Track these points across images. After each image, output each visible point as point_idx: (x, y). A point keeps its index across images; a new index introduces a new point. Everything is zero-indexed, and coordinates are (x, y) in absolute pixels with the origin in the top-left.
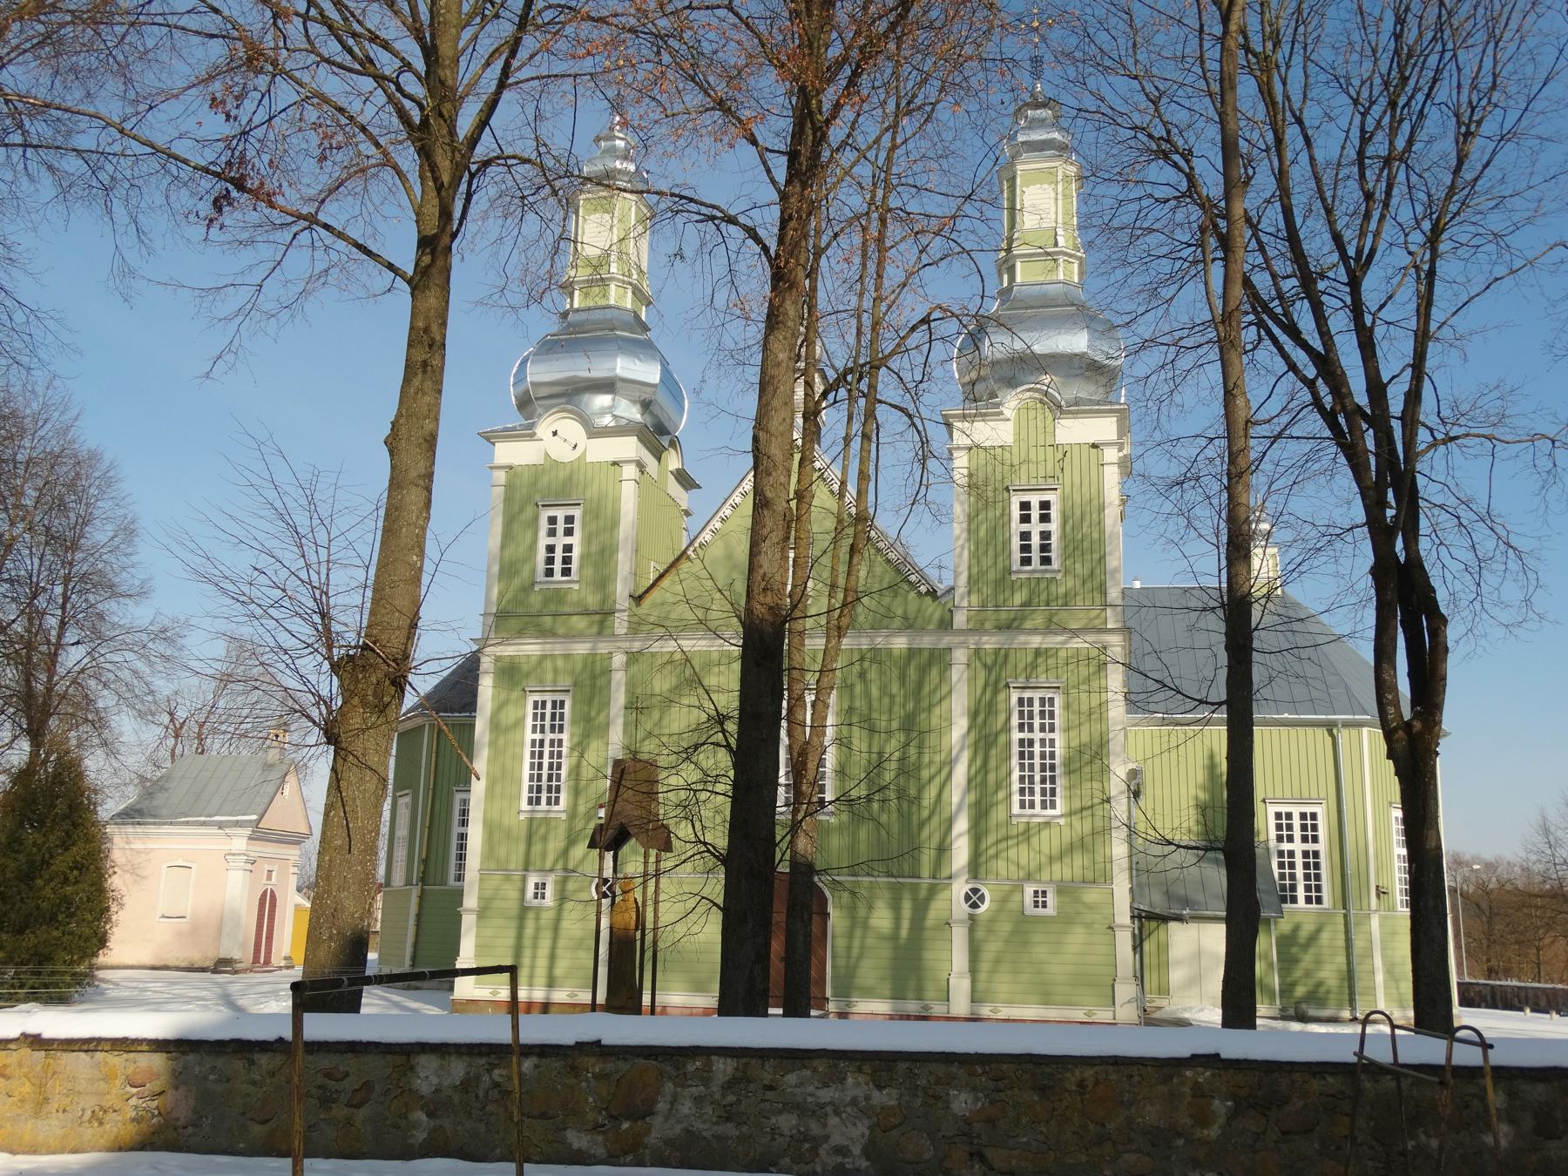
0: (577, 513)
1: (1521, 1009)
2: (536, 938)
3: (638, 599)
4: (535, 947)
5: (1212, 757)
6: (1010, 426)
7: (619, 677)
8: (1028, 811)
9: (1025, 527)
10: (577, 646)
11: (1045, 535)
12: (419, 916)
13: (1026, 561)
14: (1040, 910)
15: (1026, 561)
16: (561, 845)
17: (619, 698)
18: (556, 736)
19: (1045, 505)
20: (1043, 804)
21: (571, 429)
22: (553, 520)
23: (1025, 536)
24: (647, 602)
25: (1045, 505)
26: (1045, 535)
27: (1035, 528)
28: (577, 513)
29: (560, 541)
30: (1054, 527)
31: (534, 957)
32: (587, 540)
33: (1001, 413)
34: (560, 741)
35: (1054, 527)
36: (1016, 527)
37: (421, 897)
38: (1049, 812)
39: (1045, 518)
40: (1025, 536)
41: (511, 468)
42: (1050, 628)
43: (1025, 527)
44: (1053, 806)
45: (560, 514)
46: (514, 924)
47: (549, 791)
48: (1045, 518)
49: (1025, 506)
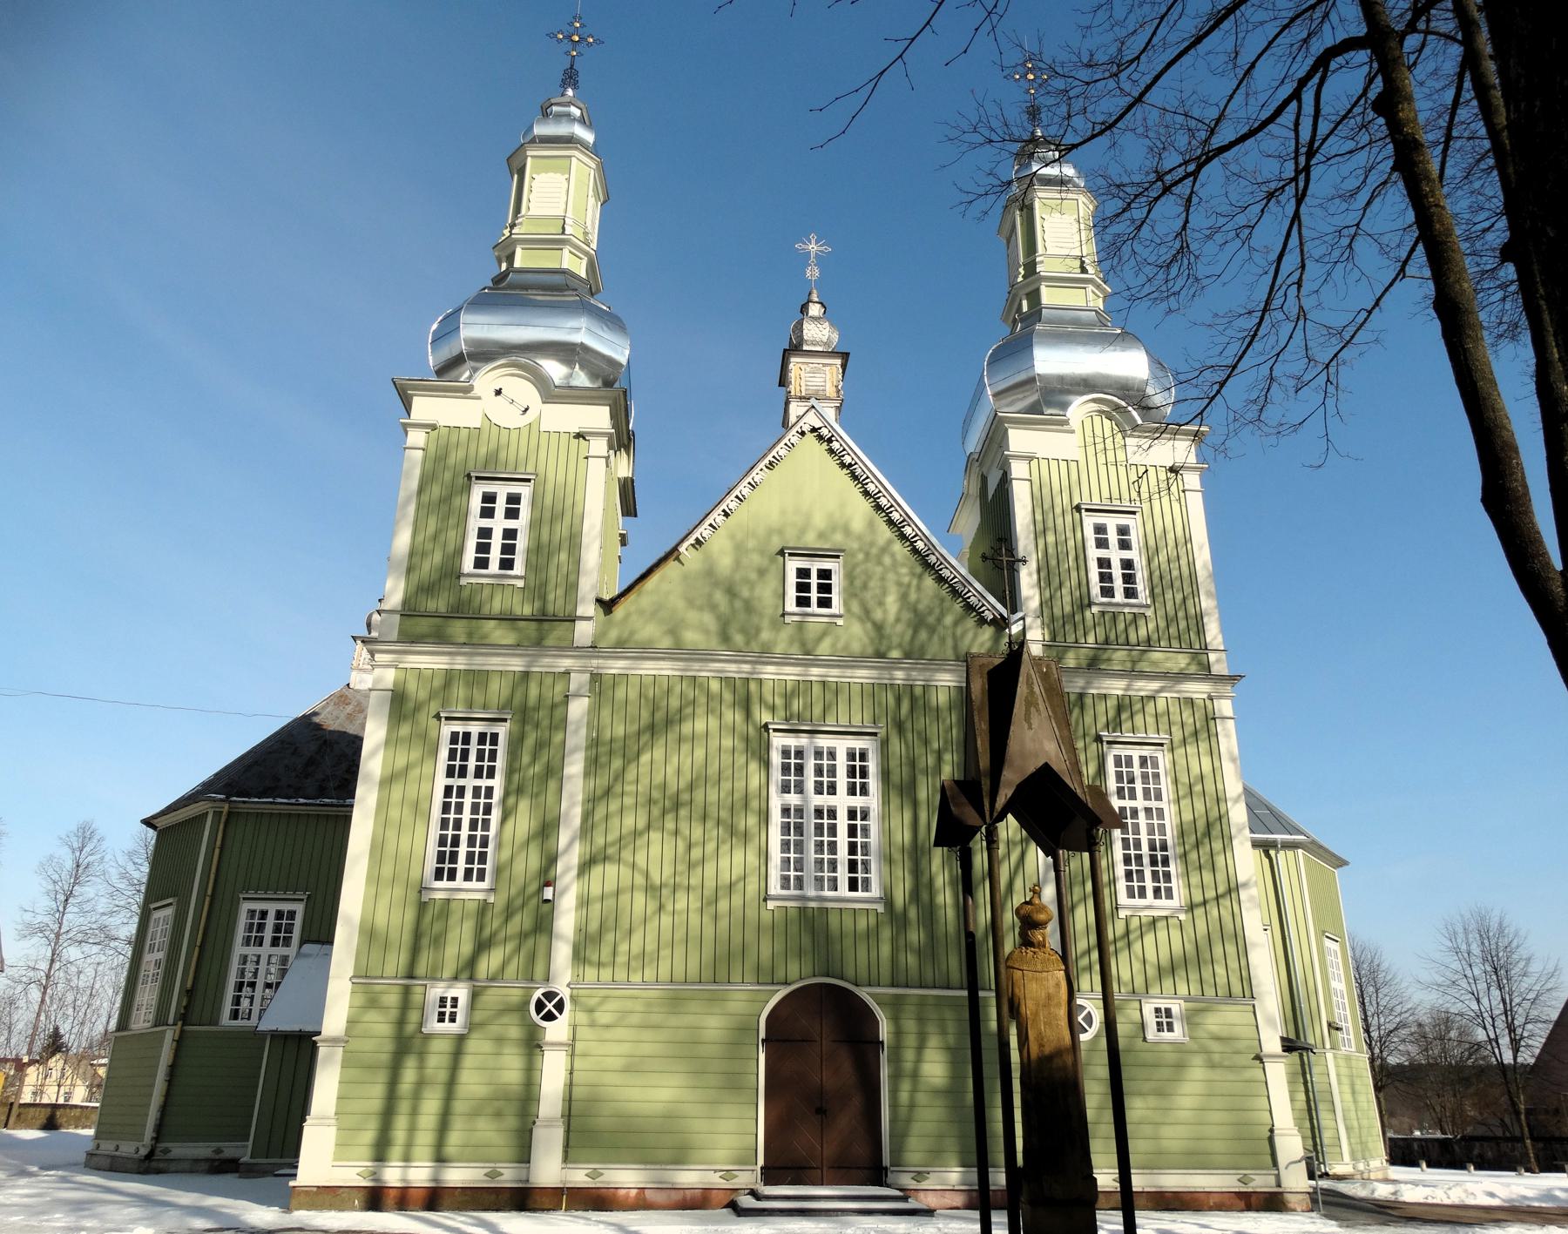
0: (525, 491)
1: (1463, 1167)
2: (417, 1096)
3: (607, 606)
4: (414, 1112)
5: (86, 835)
6: (1077, 439)
7: (578, 709)
8: (1137, 902)
9: (486, 523)
10: (610, 663)
11: (510, 534)
12: (173, 1068)
13: (481, 563)
14: (1166, 1035)
15: (481, 563)
16: (467, 949)
17: (577, 738)
18: (457, 782)
19: (514, 499)
20: (1157, 891)
21: (523, 390)
22: (489, 498)
23: (485, 533)
24: (619, 611)
25: (514, 499)
26: (510, 534)
27: (499, 524)
28: (525, 491)
29: (1115, 555)
30: (521, 524)
31: (412, 1129)
32: (535, 524)
33: (1066, 422)
34: (489, 791)
35: (521, 524)
36: (1094, 553)
37: (180, 1043)
38: (1163, 902)
39: (512, 514)
40: (1104, 563)
41: (434, 427)
42: (1133, 673)
43: (486, 523)
44: (1169, 895)
45: (502, 491)
46: (382, 1077)
47: (1139, 858)
48: (512, 514)
49: (1100, 529)
